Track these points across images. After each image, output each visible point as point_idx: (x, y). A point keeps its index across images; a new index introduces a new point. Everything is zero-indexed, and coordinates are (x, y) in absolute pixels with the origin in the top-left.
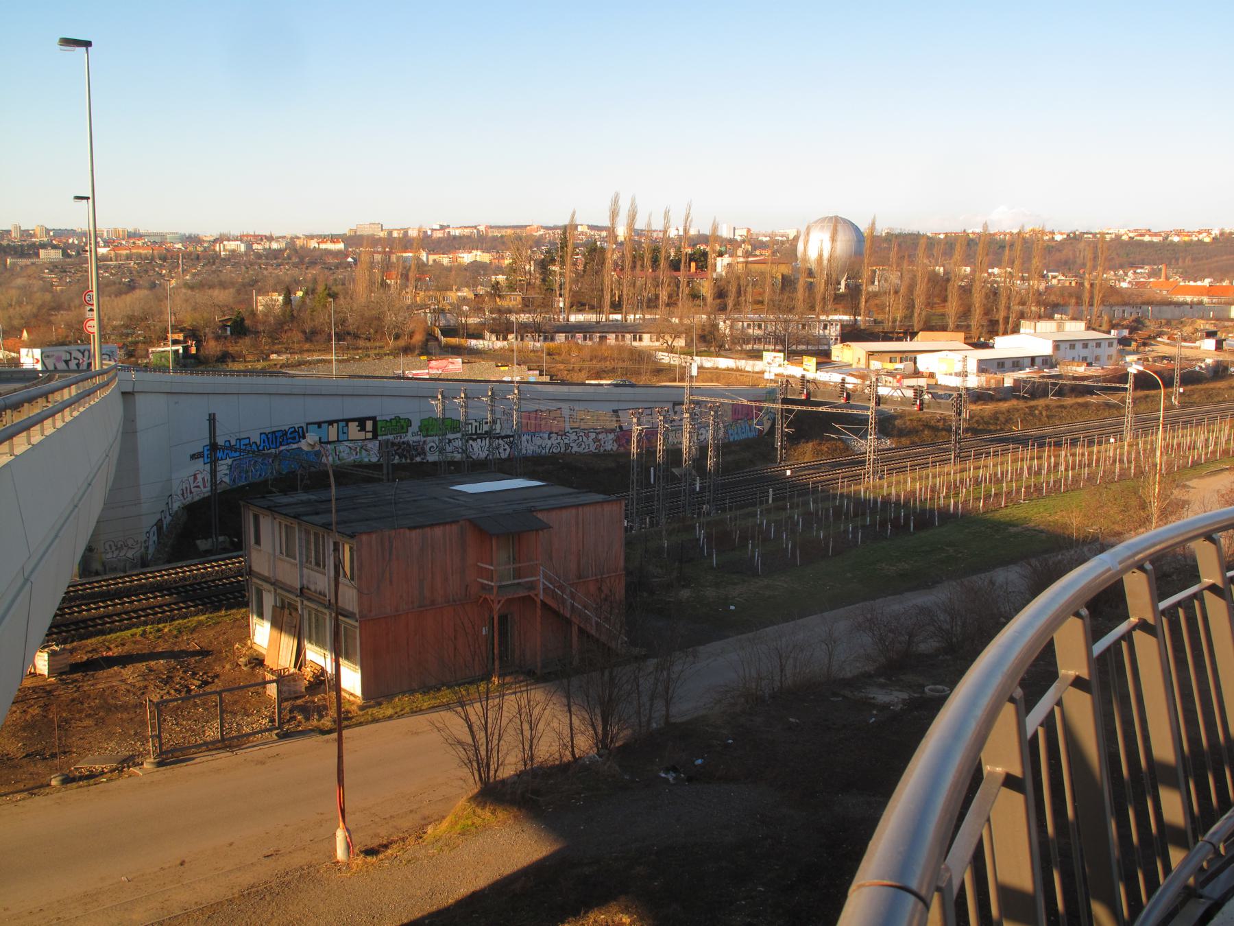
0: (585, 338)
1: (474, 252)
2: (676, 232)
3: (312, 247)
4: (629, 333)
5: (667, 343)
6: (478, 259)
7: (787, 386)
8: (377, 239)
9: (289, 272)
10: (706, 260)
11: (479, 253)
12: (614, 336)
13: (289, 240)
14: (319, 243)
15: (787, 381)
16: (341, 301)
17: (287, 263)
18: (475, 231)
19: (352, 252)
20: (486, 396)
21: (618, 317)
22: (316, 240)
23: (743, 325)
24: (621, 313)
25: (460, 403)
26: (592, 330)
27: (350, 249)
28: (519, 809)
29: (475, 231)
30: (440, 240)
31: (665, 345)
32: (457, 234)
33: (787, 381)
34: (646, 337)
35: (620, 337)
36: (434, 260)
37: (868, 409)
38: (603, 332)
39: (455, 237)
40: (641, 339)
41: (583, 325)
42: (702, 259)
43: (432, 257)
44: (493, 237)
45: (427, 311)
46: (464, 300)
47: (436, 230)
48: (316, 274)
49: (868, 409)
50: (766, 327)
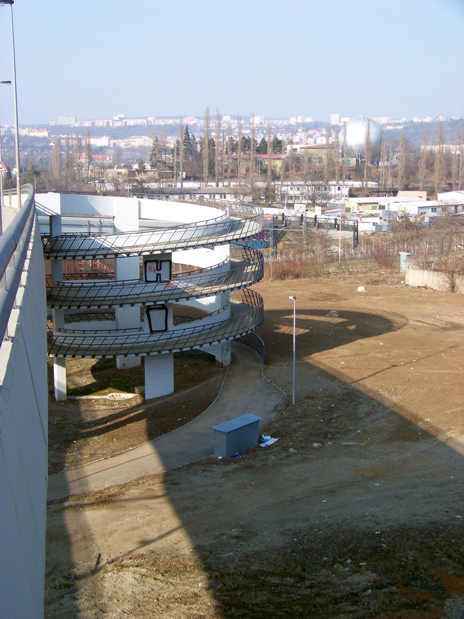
1: (144, 137)
2: (295, 121)
3: (24, 135)
4: (218, 194)
5: (240, 199)
8: (72, 128)
9: (7, 154)
12: (188, 195)
13: (6, 130)
14: (29, 132)
16: (43, 176)
17: (7, 147)
18: (145, 121)
22: (26, 129)
24: (335, 180)
27: (53, 136)
28: (217, 607)
29: (145, 121)
30: (119, 128)
31: (239, 200)
32: (132, 124)
34: (228, 196)
36: (114, 144)
37: (302, 229)
39: (130, 127)
40: (225, 198)
43: (112, 142)
44: (159, 125)
45: (97, 181)
47: (116, 121)
48: (27, 156)
49: (302, 229)
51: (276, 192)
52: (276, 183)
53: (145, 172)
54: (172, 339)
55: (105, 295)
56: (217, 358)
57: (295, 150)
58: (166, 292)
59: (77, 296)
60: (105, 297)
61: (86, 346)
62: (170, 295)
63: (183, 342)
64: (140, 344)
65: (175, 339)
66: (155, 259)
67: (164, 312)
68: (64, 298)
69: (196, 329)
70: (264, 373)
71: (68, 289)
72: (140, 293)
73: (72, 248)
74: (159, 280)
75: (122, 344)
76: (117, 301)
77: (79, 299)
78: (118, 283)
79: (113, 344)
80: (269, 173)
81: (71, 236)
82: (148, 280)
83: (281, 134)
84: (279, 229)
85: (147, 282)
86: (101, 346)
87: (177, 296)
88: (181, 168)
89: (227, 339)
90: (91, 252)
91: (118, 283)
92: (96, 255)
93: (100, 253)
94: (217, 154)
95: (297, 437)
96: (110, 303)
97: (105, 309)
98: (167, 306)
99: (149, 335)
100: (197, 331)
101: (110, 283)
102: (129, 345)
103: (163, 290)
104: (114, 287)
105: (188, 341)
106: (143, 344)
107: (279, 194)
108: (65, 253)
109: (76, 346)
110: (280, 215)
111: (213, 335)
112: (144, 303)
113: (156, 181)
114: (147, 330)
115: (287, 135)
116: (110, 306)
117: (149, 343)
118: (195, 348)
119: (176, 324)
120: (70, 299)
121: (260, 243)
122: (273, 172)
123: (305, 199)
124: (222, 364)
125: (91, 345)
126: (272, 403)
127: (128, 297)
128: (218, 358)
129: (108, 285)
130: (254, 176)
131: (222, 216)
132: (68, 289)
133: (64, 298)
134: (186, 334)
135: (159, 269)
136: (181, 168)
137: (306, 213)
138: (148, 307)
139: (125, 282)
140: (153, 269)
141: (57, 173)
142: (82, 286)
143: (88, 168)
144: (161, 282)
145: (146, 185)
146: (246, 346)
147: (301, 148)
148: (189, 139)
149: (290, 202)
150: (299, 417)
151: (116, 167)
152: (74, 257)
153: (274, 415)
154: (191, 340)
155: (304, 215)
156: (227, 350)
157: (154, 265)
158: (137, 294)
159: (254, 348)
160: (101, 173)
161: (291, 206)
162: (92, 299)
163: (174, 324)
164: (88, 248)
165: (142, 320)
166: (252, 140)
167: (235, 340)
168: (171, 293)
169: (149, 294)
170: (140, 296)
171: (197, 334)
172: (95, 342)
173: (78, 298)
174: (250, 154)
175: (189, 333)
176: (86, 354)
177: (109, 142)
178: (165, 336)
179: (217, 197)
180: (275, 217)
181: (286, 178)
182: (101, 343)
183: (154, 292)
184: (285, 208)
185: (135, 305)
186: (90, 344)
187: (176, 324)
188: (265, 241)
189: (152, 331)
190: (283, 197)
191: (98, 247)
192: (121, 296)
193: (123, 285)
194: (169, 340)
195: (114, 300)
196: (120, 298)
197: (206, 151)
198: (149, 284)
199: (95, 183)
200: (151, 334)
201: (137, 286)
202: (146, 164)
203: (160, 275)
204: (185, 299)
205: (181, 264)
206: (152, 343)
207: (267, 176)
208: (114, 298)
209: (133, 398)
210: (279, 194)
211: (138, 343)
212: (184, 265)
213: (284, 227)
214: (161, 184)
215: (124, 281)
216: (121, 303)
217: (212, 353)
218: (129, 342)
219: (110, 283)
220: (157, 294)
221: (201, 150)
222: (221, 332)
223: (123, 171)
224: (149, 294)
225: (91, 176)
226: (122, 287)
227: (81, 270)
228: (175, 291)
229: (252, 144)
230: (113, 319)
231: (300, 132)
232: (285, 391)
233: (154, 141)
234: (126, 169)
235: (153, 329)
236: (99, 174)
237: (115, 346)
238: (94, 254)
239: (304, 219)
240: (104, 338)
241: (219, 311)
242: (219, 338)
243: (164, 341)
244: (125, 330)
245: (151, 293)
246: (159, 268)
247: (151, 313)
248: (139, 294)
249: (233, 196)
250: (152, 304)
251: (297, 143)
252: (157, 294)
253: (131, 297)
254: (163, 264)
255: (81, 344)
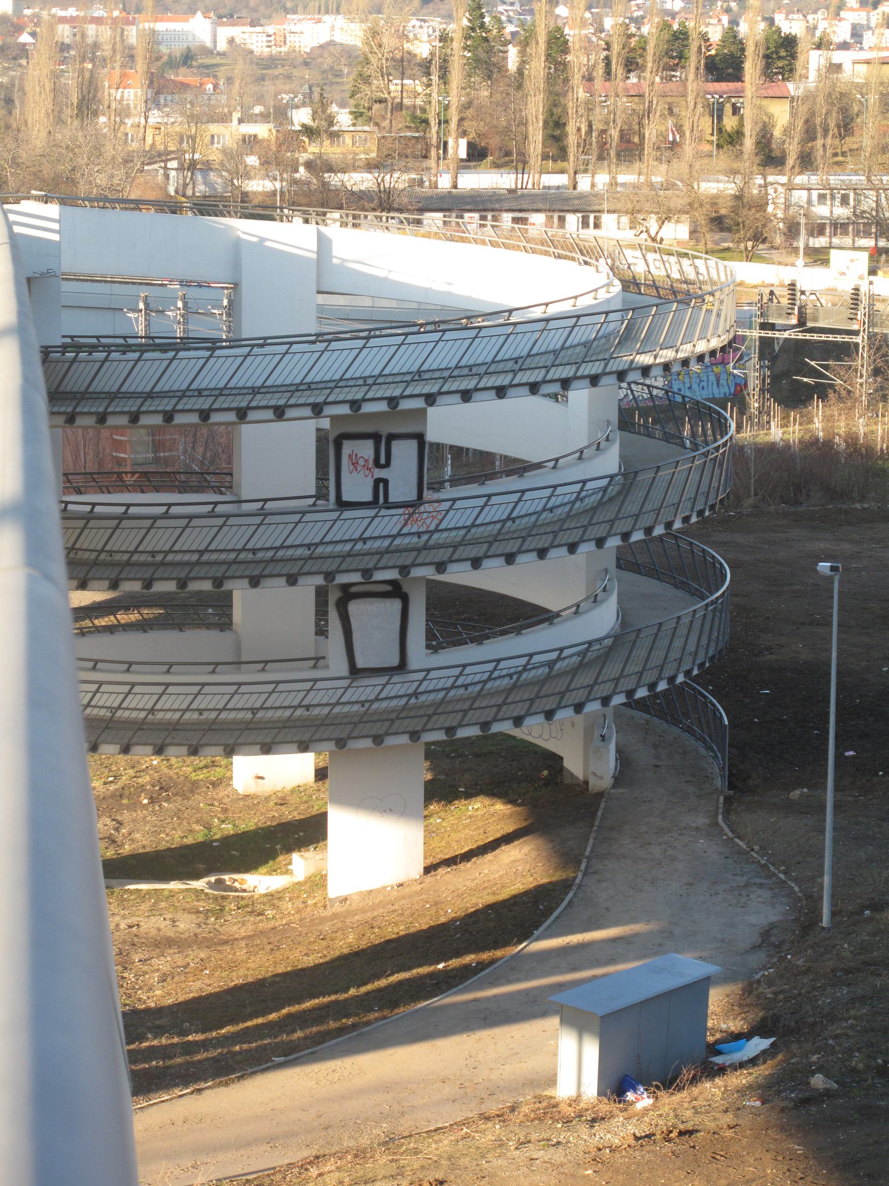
0: (585, 224)
1: (328, 19)
6: (338, 39)
7: (771, 300)
10: (793, 56)
11: (340, 21)
15: (772, 293)
19: (31, 18)
20: (220, 307)
21: (561, 180)
23: (810, 196)
25: (175, 317)
26: (497, 206)
33: (772, 293)
34: (608, 220)
35: (556, 220)
36: (231, 41)
37: (856, 333)
38: (520, 211)
40: (597, 226)
41: (479, 196)
42: (783, 53)
45: (173, 164)
46: (250, 143)
50: (858, 202)
51: (770, 208)
52: (770, 179)
53: (335, 136)
54: (422, 698)
55: (202, 547)
56: (567, 764)
57: (838, 67)
58: (407, 540)
59: (107, 548)
60: (202, 553)
61: (134, 714)
62: (419, 550)
63: (458, 707)
64: (316, 711)
65: (432, 696)
66: (369, 429)
67: (395, 605)
68: (95, 555)
69: (502, 665)
70: (725, 819)
71: (81, 523)
72: (317, 540)
73: (97, 386)
74: (381, 500)
75: (254, 711)
76: (243, 567)
77: (117, 557)
78: (246, 507)
79: (224, 709)
80: (749, 143)
81: (92, 348)
82: (345, 498)
83: (787, 15)
84: (777, 335)
85: (343, 505)
86: (187, 716)
87: (441, 555)
88: (453, 125)
89: (605, 701)
90: (157, 402)
91: (246, 507)
92: (174, 411)
93: (188, 407)
94: (576, 79)
95: (836, 1037)
96: (218, 572)
97: (198, 593)
98: (405, 589)
99: (345, 683)
100: (504, 672)
101: (220, 509)
102: (279, 713)
103: (394, 532)
104: (232, 521)
105: (476, 705)
106: (326, 710)
107: (780, 215)
108: (74, 403)
109: (103, 712)
110: (782, 285)
111: (561, 684)
112: (329, 576)
113: (370, 166)
114: (338, 665)
115: (810, 17)
116: (218, 582)
117: (346, 709)
118: (496, 728)
119: (434, 644)
120: (86, 555)
121: (712, 378)
122: (764, 142)
123: (867, 234)
124: (586, 783)
125: (152, 711)
126: (753, 919)
127: (280, 553)
128: (574, 765)
129: (212, 515)
130: (699, 155)
131: (596, 290)
132: (81, 523)
133: (95, 555)
134: (469, 680)
135: (383, 461)
136: (453, 125)
137: (871, 283)
138: (345, 587)
139: (269, 505)
140: (361, 462)
141: (44, 134)
142: (125, 516)
143: (146, 118)
144: (389, 506)
145: (334, 179)
146: (665, 725)
147: (855, 62)
148: (482, 26)
149: (820, 242)
150: (847, 972)
151: (236, 116)
152: (102, 419)
153: (760, 957)
154: (484, 703)
155: (864, 289)
156: (603, 738)
157: (366, 449)
158: (308, 546)
159: (692, 733)
160: (189, 137)
161: (819, 257)
162: (159, 558)
163: (428, 647)
164: (148, 389)
165: (321, 631)
166: (693, 35)
167: (632, 703)
168: (421, 544)
169: (348, 547)
170: (320, 550)
171: (506, 681)
172: (166, 702)
173: (111, 553)
174: (684, 82)
175: (477, 678)
176: (132, 741)
177: (215, 36)
178: (399, 686)
179: (572, 220)
180: (767, 291)
181: (806, 162)
182: (184, 706)
183: (365, 540)
184: (800, 261)
185: (302, 580)
186: (149, 706)
187: (434, 644)
188: (731, 374)
189: (355, 672)
190: (792, 230)
191: (184, 387)
192: (254, 551)
193: (263, 514)
194: (413, 701)
195: (230, 564)
196: (250, 556)
197: (538, 68)
198: (347, 514)
199: (166, 168)
200: (353, 680)
201: (308, 517)
202: (334, 108)
203: (386, 482)
204: (467, 565)
205: (451, 447)
206: (356, 708)
207: (739, 155)
208: (232, 556)
209: (285, 890)
210: (780, 215)
211: (308, 707)
212: (506, 457)
213: (794, 327)
214: (388, 177)
215: (266, 501)
216: (256, 572)
217: (551, 746)
218: (277, 704)
219: (220, 509)
220: (377, 544)
221: (523, 63)
222: (584, 679)
223: (263, 130)
224: (348, 547)
225: (153, 145)
226: (258, 520)
227: (119, 462)
228: (436, 536)
229: (694, 48)
230: (225, 623)
231: (852, 9)
232: (796, 880)
233: (365, 31)
234: (271, 126)
235: (361, 663)
236: (181, 142)
237: (232, 715)
238: (169, 408)
239: (864, 301)
240: (196, 689)
241: (578, 606)
242: (577, 696)
243: (394, 703)
244: (266, 662)
245: (356, 541)
246: (383, 460)
247: (354, 608)
248: (317, 545)
249: (625, 220)
250: (356, 577)
251: (844, 46)
252: (377, 544)
253: (290, 552)
254: (398, 448)
255: (119, 708)
